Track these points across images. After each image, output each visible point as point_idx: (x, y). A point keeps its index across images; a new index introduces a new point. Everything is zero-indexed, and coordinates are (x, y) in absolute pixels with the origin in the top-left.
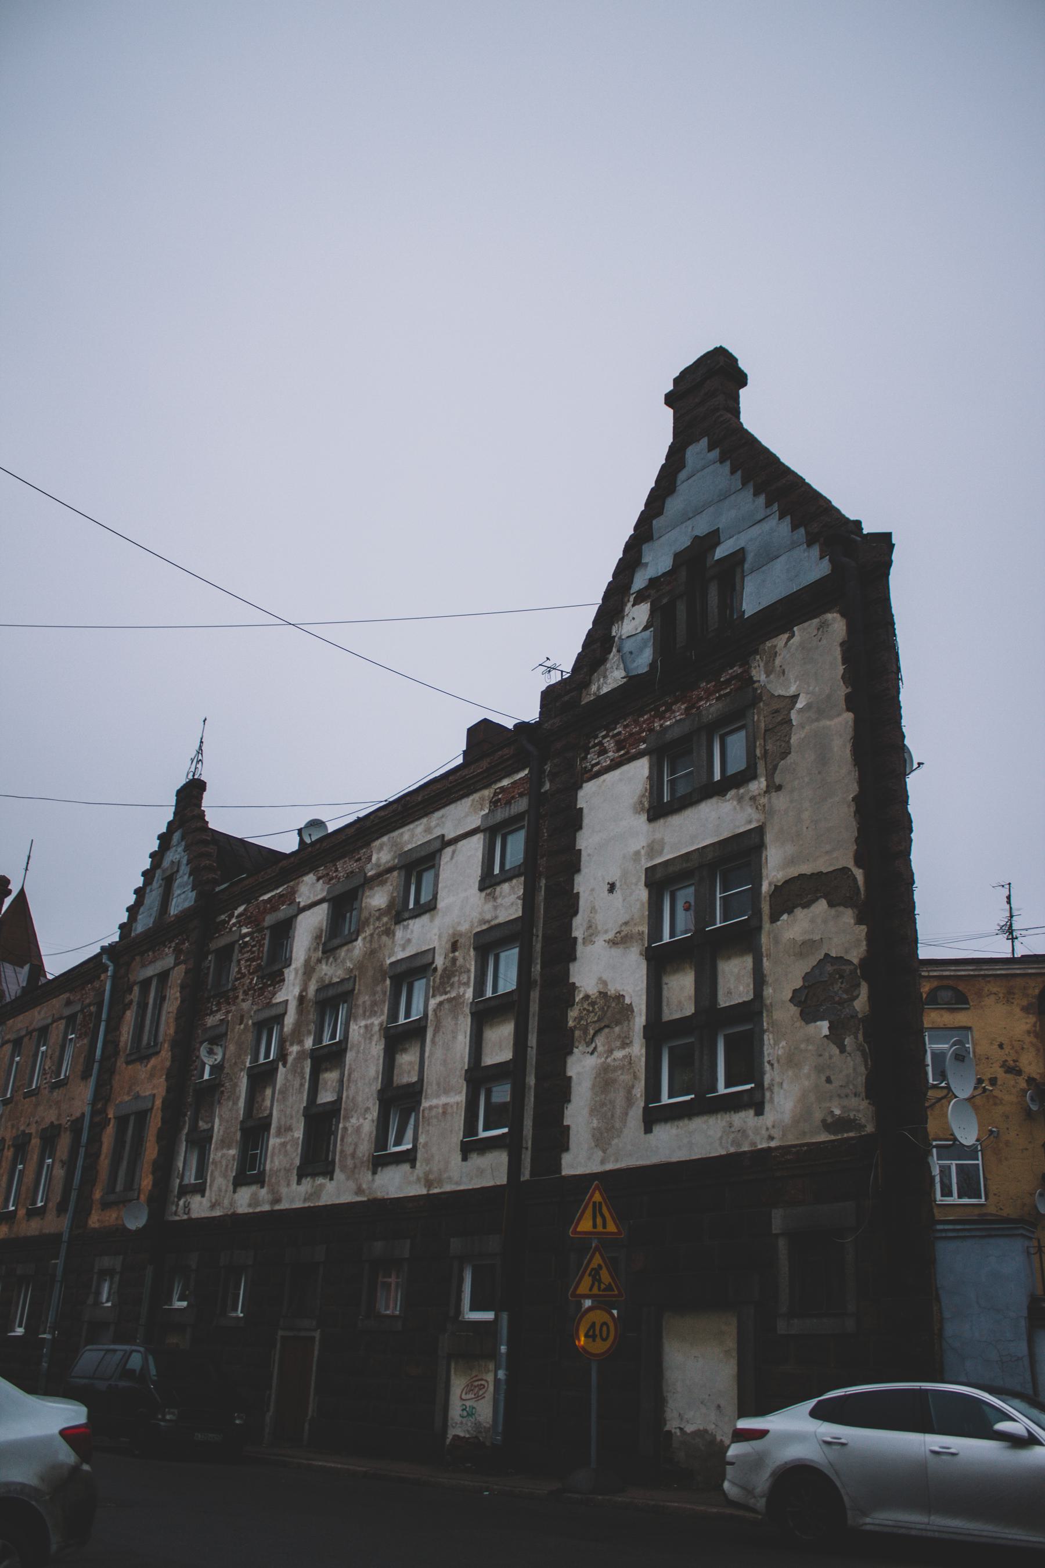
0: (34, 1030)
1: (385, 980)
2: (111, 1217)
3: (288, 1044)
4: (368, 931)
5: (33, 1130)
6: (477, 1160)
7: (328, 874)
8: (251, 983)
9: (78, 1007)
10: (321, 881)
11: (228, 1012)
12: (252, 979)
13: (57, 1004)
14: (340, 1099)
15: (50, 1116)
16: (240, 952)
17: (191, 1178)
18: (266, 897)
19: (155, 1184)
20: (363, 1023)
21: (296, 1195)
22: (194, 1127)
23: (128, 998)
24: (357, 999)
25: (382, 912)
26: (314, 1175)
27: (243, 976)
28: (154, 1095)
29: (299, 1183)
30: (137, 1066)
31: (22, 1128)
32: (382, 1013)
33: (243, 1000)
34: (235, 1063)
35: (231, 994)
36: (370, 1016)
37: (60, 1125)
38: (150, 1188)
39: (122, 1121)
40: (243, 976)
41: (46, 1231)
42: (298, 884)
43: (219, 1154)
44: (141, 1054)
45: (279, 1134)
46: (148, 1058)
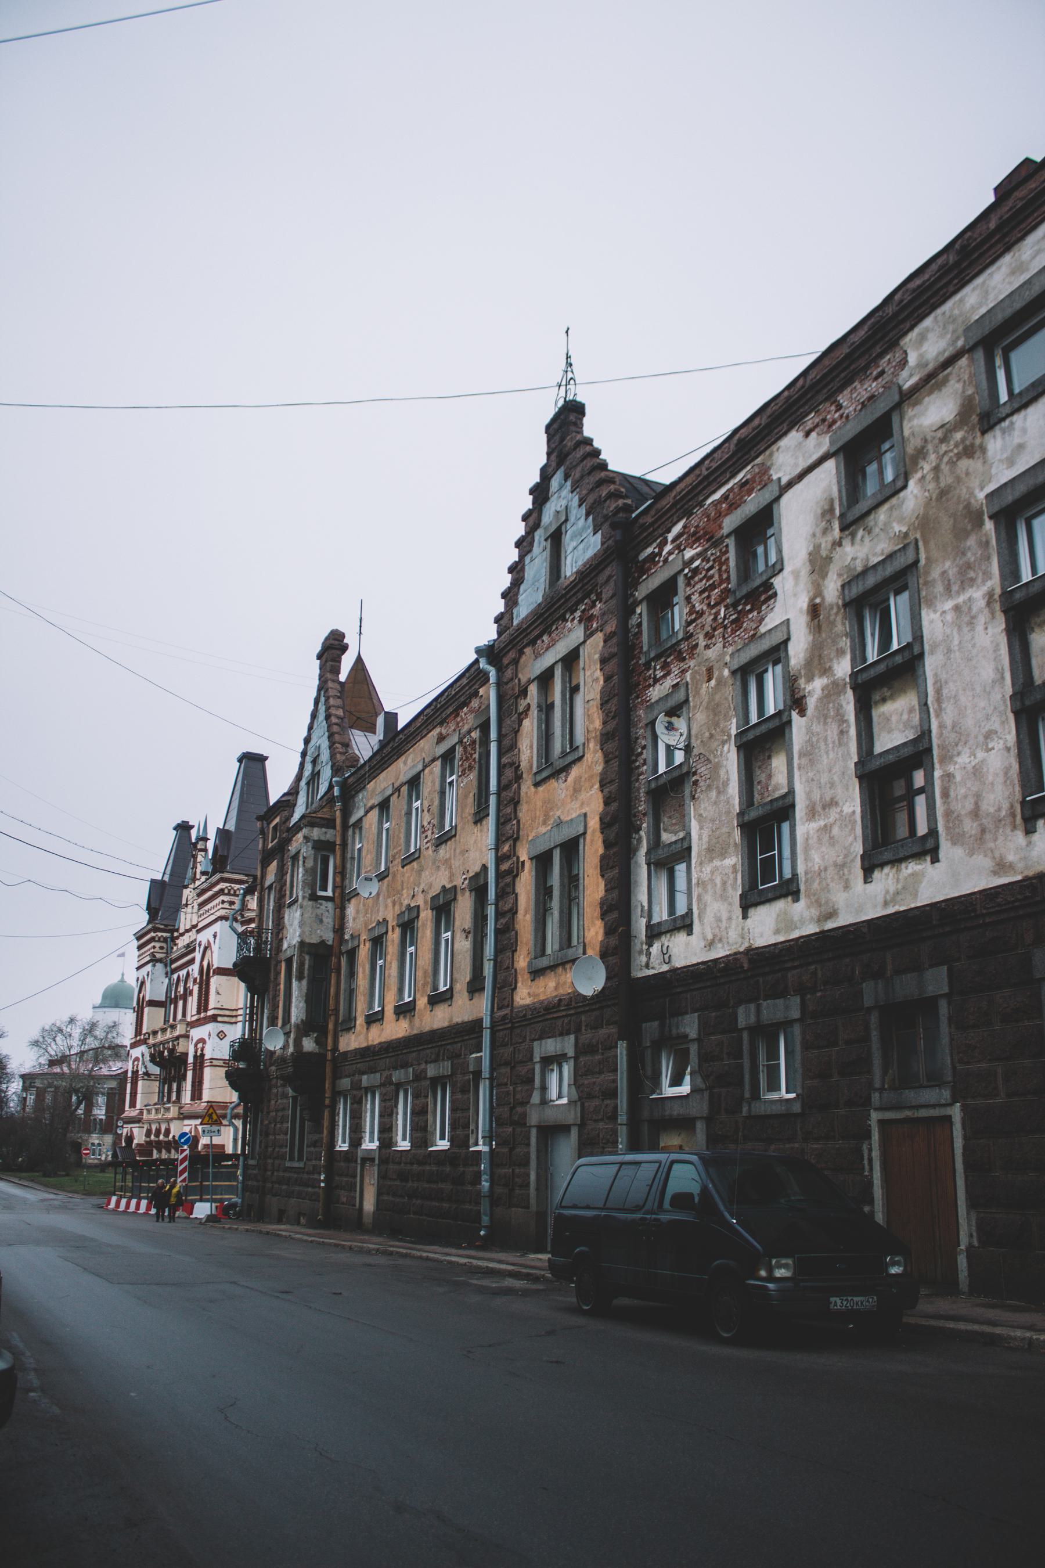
0: (402, 785)
1: (981, 524)
2: (548, 988)
3: (802, 682)
4: (926, 467)
5: (420, 901)
6: (541, 981)
7: (824, 420)
8: (715, 619)
9: (455, 739)
10: (814, 434)
11: (683, 672)
12: (718, 613)
13: (427, 746)
14: (925, 734)
15: (437, 880)
16: (688, 584)
17: (661, 914)
18: (717, 496)
19: (609, 932)
20: (949, 605)
21: (866, 899)
22: (656, 843)
23: (522, 704)
24: (927, 573)
25: (946, 430)
26: (896, 861)
27: (701, 614)
28: (585, 815)
29: (867, 878)
30: (553, 783)
31: (406, 902)
32: (987, 575)
33: (707, 647)
34: (711, 736)
35: (684, 646)
36: (962, 589)
37: (455, 887)
38: (600, 937)
39: (543, 861)
40: (701, 614)
41: (458, 1019)
42: (771, 455)
43: (708, 869)
44: (553, 770)
45: (812, 813)
46: (566, 769)
